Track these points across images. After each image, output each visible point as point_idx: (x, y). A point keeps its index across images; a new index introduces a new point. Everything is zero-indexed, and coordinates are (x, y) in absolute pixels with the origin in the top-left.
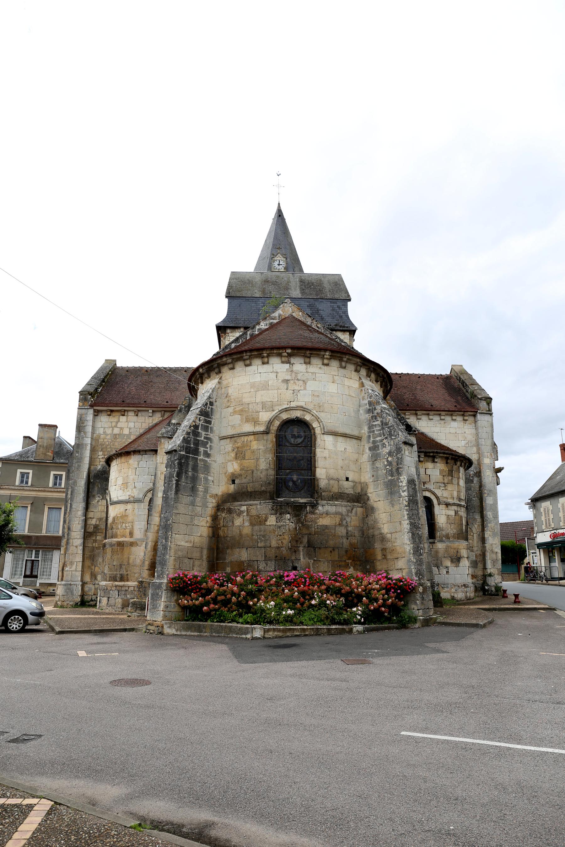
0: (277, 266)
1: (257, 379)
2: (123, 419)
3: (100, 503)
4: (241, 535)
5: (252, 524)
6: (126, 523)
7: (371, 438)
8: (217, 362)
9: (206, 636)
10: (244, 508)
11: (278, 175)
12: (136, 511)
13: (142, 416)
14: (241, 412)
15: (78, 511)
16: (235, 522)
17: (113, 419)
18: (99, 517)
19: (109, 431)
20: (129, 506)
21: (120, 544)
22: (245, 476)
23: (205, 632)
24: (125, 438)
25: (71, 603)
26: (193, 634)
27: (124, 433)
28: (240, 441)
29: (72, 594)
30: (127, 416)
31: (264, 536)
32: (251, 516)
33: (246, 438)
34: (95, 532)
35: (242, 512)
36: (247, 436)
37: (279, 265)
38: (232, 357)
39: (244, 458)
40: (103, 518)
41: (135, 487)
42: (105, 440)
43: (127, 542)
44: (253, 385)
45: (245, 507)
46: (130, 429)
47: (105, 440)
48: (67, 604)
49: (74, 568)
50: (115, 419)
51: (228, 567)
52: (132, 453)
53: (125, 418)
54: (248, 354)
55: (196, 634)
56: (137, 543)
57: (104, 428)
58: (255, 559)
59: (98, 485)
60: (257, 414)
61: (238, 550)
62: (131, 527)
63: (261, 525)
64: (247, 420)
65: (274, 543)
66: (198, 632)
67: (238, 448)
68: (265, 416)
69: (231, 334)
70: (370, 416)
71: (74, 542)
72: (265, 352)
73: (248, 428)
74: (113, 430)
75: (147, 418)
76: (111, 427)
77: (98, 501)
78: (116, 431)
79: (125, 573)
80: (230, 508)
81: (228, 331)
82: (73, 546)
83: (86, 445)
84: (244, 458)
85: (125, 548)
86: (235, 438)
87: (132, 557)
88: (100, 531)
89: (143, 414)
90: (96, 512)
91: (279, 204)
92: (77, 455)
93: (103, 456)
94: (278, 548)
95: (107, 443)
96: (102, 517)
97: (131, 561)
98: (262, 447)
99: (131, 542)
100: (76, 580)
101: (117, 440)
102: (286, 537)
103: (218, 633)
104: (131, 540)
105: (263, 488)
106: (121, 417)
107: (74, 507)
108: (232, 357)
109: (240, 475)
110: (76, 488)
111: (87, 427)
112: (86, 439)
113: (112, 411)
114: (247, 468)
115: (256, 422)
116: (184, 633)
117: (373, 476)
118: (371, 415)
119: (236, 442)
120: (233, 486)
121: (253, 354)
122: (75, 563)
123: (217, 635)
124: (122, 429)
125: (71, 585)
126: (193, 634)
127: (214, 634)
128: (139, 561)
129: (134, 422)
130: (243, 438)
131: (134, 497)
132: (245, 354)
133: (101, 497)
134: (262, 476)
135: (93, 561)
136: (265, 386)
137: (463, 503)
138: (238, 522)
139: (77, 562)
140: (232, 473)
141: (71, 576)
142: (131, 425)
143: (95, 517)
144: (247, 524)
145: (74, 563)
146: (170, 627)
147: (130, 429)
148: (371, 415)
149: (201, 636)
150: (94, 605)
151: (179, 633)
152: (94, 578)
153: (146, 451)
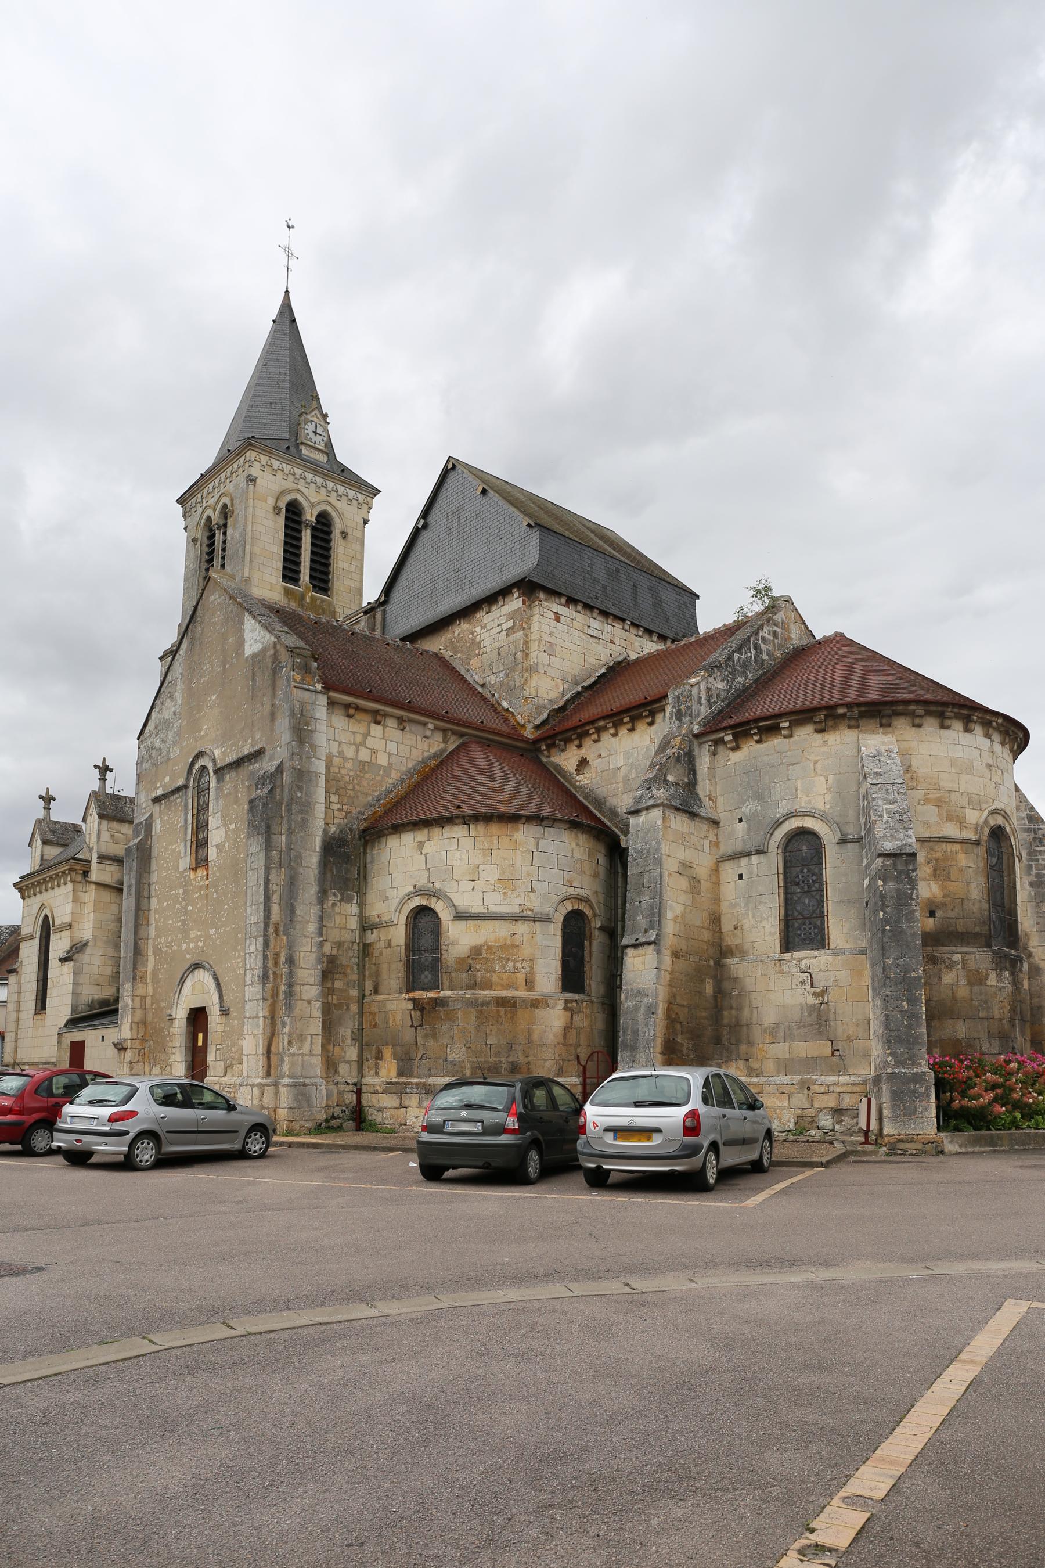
0: (312, 435)
1: (959, 753)
2: (376, 730)
3: (337, 909)
4: (954, 998)
5: (970, 983)
6: (515, 961)
7: (1034, 869)
8: (894, 708)
9: (1004, 1151)
10: (957, 957)
11: (289, 227)
12: (539, 938)
13: (411, 732)
14: (939, 803)
15: (308, 922)
16: (944, 978)
17: (358, 726)
18: (337, 939)
19: (350, 752)
20: (522, 928)
21: (501, 1002)
22: (952, 907)
23: (1002, 1146)
24: (381, 772)
25: (309, 1125)
26: (983, 1149)
27: (379, 762)
28: (940, 849)
29: (310, 1105)
30: (385, 726)
31: (986, 1002)
32: (970, 971)
33: (949, 847)
34: (330, 972)
35: (955, 963)
36: (951, 844)
37: (316, 433)
38: (927, 708)
39: (949, 879)
40: (344, 942)
41: (533, 890)
42: (343, 771)
43: (524, 1000)
44: (953, 762)
45: (959, 956)
46: (390, 755)
47: (343, 771)
48: (301, 1127)
49: (306, 1048)
50: (361, 729)
51: (937, 1047)
52: (524, 820)
53: (379, 728)
54: (956, 710)
55: (988, 1149)
56: (546, 1001)
57: (340, 743)
58: (976, 1035)
59: (331, 870)
60: (963, 810)
61: (950, 1021)
62: (528, 969)
63: (981, 984)
64: (950, 818)
65: (997, 1014)
66: (990, 1146)
67: (937, 860)
68: (973, 817)
69: (546, 604)
70: (1031, 837)
71: (304, 991)
72: (976, 714)
73: (951, 830)
74: (357, 751)
75: (419, 738)
76: (354, 744)
77: (334, 905)
78: (364, 755)
79: (522, 1059)
80: (933, 956)
81: (542, 595)
82: (301, 1000)
83: (318, 775)
84: (949, 879)
85: (520, 1012)
86: (931, 844)
87: (537, 1030)
88: (339, 970)
89: (413, 729)
90: (332, 928)
91: (287, 292)
92: (299, 795)
93: (339, 806)
94: (1001, 1020)
95: (347, 778)
96: (343, 939)
97: (535, 1037)
98: (971, 865)
99: (532, 1000)
100: (312, 1074)
101: (367, 776)
102: (1007, 1004)
103: (1023, 1145)
104: (533, 995)
105: (978, 929)
106: (373, 725)
107: (298, 912)
108: (927, 708)
109: (944, 905)
110: (301, 870)
111: (316, 735)
112: (317, 762)
113: (357, 708)
114: (955, 894)
115: (962, 823)
116: (970, 1150)
117: (1038, 924)
118: (1032, 835)
119: (932, 849)
120: (931, 920)
121: (962, 711)
122: (309, 1037)
123: (1022, 1148)
124: (374, 752)
125: (305, 1085)
126: (983, 1149)
127: (1016, 1147)
128: (551, 1036)
129: (397, 743)
130: (944, 845)
131: (532, 910)
132: (949, 709)
133: (339, 898)
134: (975, 910)
135: (330, 1033)
136: (968, 769)
137: (443, 947)
138: (948, 978)
139: (312, 1035)
140: (928, 899)
141: (302, 1065)
142: (392, 747)
143: (330, 939)
144: (963, 982)
145: (306, 1038)
146: (951, 1142)
147: (390, 755)
148: (1032, 835)
149: (995, 1151)
150: (338, 1127)
151: (963, 1150)
152: (332, 1071)
153: (555, 820)
